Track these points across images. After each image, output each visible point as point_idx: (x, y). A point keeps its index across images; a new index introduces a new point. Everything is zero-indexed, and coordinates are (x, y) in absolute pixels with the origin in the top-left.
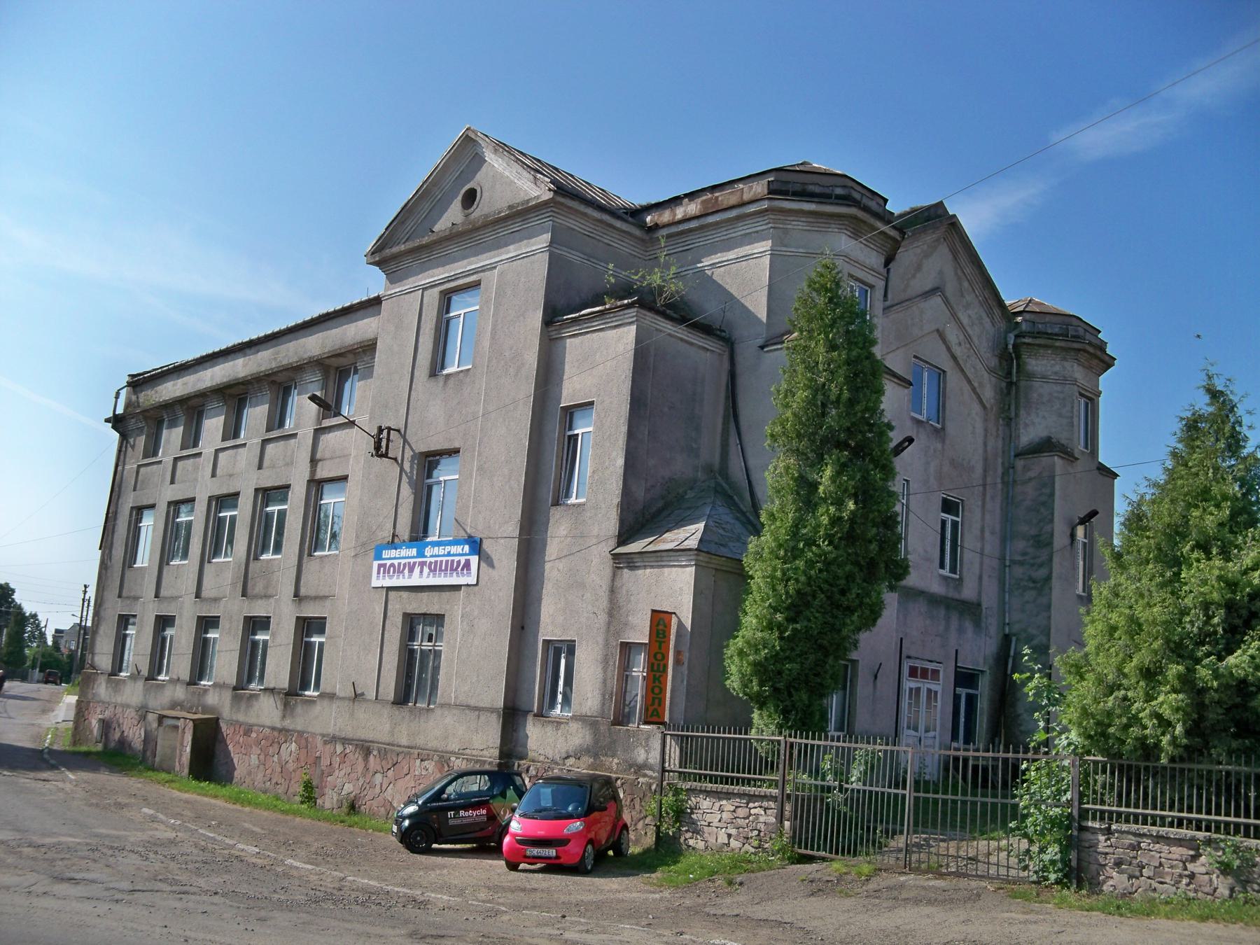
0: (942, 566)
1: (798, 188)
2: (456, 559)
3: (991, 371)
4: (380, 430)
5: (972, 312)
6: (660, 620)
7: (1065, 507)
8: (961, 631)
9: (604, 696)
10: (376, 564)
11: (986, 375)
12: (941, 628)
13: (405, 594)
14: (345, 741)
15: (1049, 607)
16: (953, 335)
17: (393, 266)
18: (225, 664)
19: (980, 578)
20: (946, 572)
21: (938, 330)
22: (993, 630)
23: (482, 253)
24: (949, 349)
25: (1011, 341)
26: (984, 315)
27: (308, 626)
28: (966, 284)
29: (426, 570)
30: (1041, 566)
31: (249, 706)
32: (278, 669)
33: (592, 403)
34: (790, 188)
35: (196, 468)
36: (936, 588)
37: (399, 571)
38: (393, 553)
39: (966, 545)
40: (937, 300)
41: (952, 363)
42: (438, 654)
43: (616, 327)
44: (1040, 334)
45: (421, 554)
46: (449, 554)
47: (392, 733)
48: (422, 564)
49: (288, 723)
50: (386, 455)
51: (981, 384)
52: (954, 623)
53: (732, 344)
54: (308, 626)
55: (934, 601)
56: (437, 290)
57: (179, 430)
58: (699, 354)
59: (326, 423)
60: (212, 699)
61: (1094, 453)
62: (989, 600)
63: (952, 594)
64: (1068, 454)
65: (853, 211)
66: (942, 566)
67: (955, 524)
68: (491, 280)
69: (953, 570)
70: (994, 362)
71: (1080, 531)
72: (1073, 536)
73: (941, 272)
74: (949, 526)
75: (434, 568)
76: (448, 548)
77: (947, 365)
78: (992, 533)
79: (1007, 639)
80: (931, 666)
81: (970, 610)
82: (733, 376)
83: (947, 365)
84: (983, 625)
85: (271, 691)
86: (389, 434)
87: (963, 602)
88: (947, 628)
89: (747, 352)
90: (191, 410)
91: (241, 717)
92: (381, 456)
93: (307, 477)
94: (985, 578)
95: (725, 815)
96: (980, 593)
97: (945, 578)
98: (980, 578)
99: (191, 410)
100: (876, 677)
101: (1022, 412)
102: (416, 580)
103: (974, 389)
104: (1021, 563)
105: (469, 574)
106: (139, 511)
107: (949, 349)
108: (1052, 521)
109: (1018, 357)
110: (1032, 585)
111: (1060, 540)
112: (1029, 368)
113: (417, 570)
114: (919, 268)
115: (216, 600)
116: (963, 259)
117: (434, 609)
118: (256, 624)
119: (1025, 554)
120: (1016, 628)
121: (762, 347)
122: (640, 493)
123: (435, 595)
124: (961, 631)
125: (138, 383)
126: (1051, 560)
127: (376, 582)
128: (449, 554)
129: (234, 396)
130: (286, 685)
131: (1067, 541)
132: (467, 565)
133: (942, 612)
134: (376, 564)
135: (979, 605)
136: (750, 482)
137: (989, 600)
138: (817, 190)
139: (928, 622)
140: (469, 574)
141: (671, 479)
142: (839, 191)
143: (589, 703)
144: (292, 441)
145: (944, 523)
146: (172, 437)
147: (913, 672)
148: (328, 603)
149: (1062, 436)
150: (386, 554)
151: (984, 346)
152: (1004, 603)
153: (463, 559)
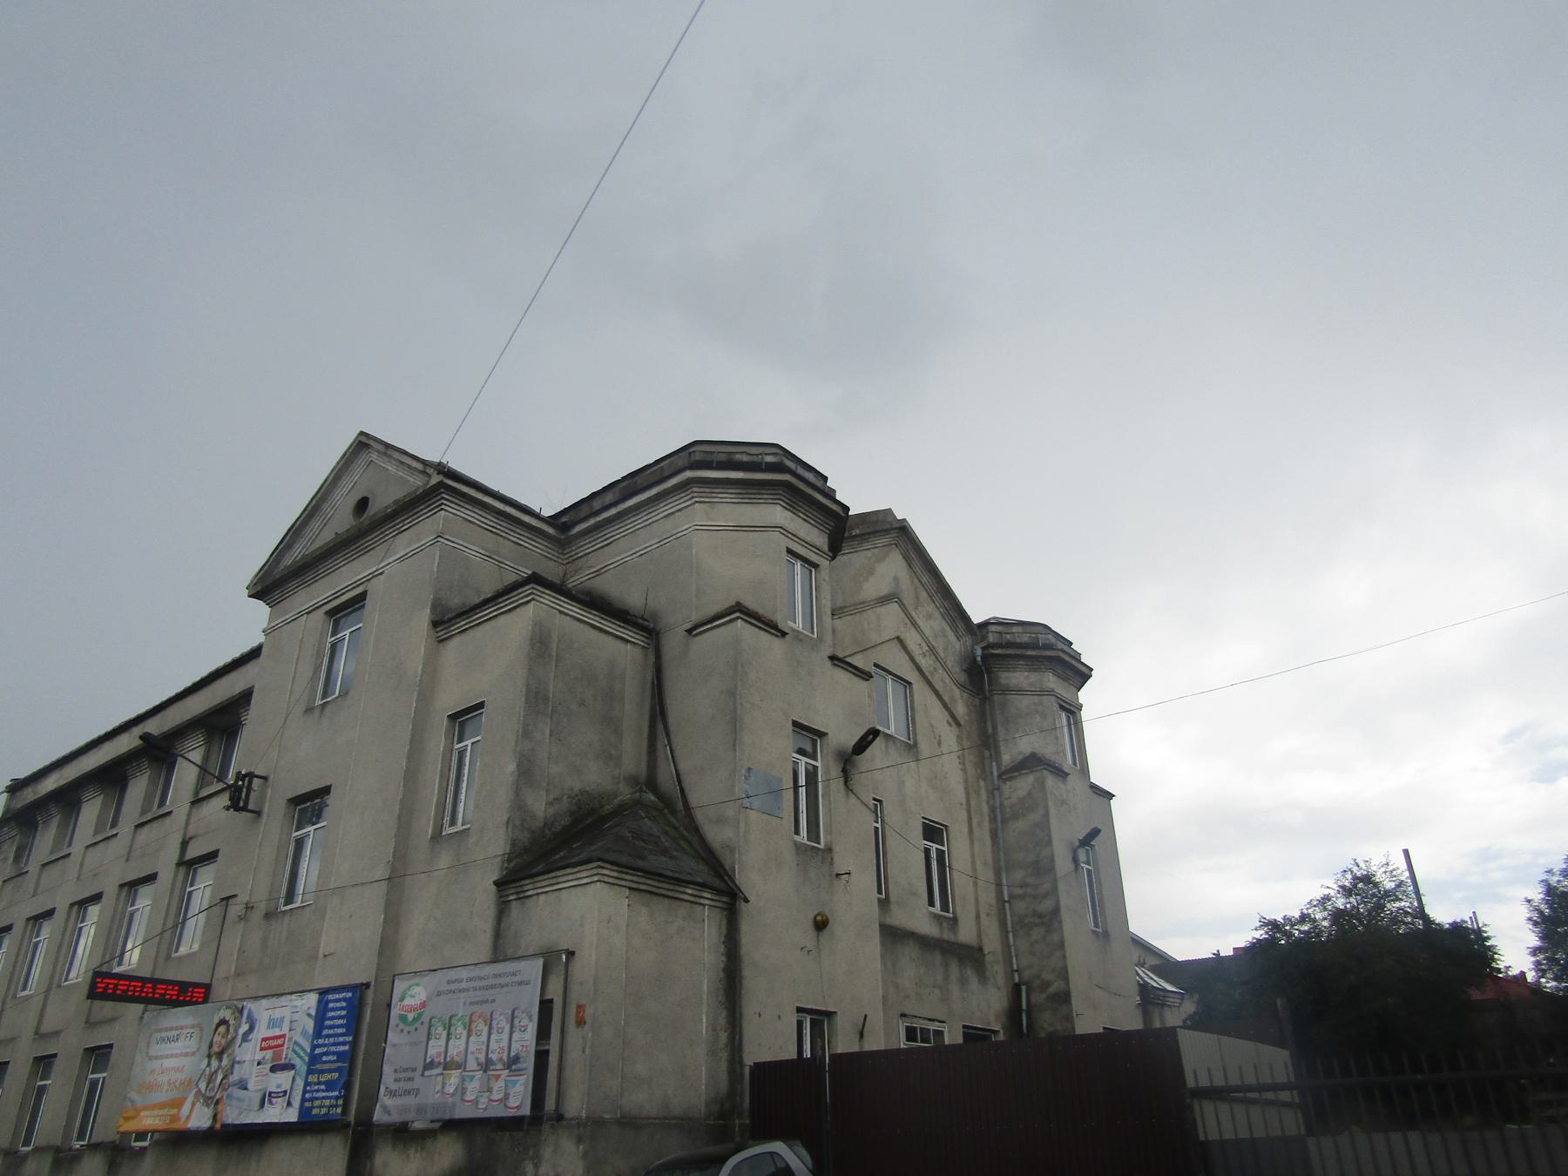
0: (931, 903)
1: (723, 458)
3: (962, 686)
5: (933, 622)
7: (1064, 833)
8: (963, 982)
11: (957, 692)
12: (940, 977)
15: (1061, 945)
16: (912, 639)
17: (276, 595)
19: (978, 916)
20: (937, 909)
21: (898, 638)
22: (1001, 979)
24: (912, 659)
25: (979, 652)
26: (947, 628)
28: (924, 594)
30: (1045, 897)
33: (481, 705)
34: (716, 458)
36: (926, 927)
39: (955, 866)
40: (894, 607)
41: (916, 673)
44: (1009, 645)
50: (245, 809)
51: (952, 698)
52: (954, 971)
53: (658, 634)
55: (924, 942)
56: (319, 615)
58: (618, 652)
61: (1085, 771)
62: (992, 944)
63: (947, 936)
64: (1061, 774)
65: (787, 477)
66: (931, 903)
67: (940, 854)
68: (376, 589)
69: (945, 907)
70: (962, 677)
71: (1082, 856)
72: (1075, 860)
73: (896, 579)
74: (934, 855)
77: (912, 676)
78: (985, 864)
79: (1016, 989)
80: (933, 1026)
81: (971, 956)
82: (659, 671)
83: (912, 676)
84: (988, 974)
86: (250, 783)
87: (962, 946)
88: (946, 978)
89: (673, 642)
90: (68, 799)
92: (237, 809)
94: (983, 916)
96: (979, 936)
97: (935, 916)
98: (978, 916)
99: (68, 799)
100: (862, 1035)
101: (1000, 728)
103: (945, 705)
104: (1022, 897)
107: (912, 659)
108: (1049, 843)
109: (989, 672)
110: (1037, 921)
111: (1063, 865)
112: (1003, 681)
114: (871, 572)
115: (57, 1033)
116: (916, 563)
119: (1023, 885)
120: (1027, 974)
121: (689, 631)
124: (963, 982)
125: (16, 787)
126: (1055, 888)
129: (112, 777)
131: (1071, 866)
133: (938, 958)
135: (980, 949)
136: (682, 790)
137: (992, 944)
138: (745, 458)
139: (922, 971)
141: (582, 792)
142: (769, 459)
144: (168, 820)
145: (927, 851)
149: (1048, 751)
151: (952, 661)
152: (1009, 947)
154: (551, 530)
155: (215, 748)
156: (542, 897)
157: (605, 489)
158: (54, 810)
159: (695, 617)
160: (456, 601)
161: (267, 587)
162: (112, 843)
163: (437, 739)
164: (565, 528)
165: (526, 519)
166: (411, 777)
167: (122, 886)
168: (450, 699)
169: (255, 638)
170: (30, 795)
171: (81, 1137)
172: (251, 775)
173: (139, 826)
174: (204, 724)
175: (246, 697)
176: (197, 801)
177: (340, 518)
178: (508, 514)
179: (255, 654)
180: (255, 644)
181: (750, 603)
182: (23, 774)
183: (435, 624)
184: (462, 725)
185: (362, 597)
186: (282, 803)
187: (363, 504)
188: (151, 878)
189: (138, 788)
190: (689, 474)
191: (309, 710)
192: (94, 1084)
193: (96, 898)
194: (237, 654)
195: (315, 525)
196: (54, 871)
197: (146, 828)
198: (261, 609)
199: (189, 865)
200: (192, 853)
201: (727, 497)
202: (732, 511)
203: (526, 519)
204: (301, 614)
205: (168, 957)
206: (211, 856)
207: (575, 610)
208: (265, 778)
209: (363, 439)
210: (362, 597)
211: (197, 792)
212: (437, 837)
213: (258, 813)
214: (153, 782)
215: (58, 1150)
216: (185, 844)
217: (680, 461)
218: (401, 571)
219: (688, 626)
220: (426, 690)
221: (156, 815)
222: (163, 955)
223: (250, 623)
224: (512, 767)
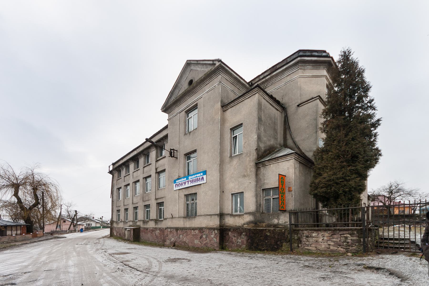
2: (199, 177)
4: (171, 150)
6: (282, 178)
9: (257, 206)
10: (174, 185)
13: (184, 190)
14: (170, 228)
18: (141, 215)
23: (179, 249)
27: (160, 204)
29: (190, 182)
31: (147, 224)
32: (153, 215)
33: (242, 124)
35: (129, 178)
37: (181, 184)
38: (179, 181)
42: (196, 203)
43: (249, 98)
45: (187, 179)
46: (196, 177)
47: (184, 224)
48: (188, 181)
49: (157, 226)
50: (173, 157)
54: (160, 204)
56: (184, 112)
57: (124, 169)
59: (158, 159)
60: (138, 224)
68: (200, 103)
75: (192, 182)
76: (196, 176)
85: (152, 220)
89: (291, 110)
91: (145, 226)
93: (155, 171)
95: (325, 238)
99: (126, 164)
102: (187, 185)
105: (204, 180)
106: (119, 189)
113: (187, 183)
115: (137, 203)
117: (193, 192)
118: (147, 206)
121: (298, 106)
122: (262, 146)
123: (194, 188)
125: (113, 164)
127: (175, 189)
128: (196, 177)
130: (156, 218)
132: (203, 178)
134: (174, 185)
140: (204, 180)
143: (251, 208)
144: (151, 165)
146: (123, 173)
147: (236, 211)
148: (164, 198)
150: (177, 181)
153: (201, 177)
154: (247, 85)
155: (158, 150)
156: (272, 165)
157: (268, 70)
158: (123, 167)
159: (299, 102)
160: (226, 102)
161: (167, 108)
162: (139, 171)
163: (228, 136)
164: (252, 85)
165: (242, 81)
166: (222, 143)
167: (143, 178)
168: (229, 124)
169: (166, 123)
170: (117, 165)
171: (147, 218)
172: (173, 150)
173: (144, 167)
174: (157, 143)
175: (166, 137)
176: (157, 161)
177: (185, 86)
178: (236, 79)
179: (166, 127)
180: (166, 125)
181: (321, 96)
182: (114, 162)
183: (222, 107)
184: (233, 131)
185: (196, 105)
186: (183, 156)
187: (191, 82)
188: (150, 176)
189: (142, 161)
190: (299, 59)
191: (185, 134)
192: (147, 211)
193: (138, 181)
194: (159, 130)
195: (177, 91)
196: (127, 177)
197: (146, 168)
198: (166, 116)
199: (158, 173)
200: (158, 170)
201: (310, 67)
202: (310, 72)
203: (242, 81)
204: (177, 114)
205: (158, 189)
206: (164, 171)
207: (267, 98)
208: (177, 151)
209: (189, 62)
210: (196, 105)
211: (156, 159)
212: (231, 156)
213: (177, 158)
214: (145, 159)
215: (143, 221)
216: (156, 169)
217: (297, 55)
218: (209, 95)
219: (298, 104)
220: (223, 121)
221: (147, 164)
222: (157, 189)
223: (162, 120)
224: (256, 136)
